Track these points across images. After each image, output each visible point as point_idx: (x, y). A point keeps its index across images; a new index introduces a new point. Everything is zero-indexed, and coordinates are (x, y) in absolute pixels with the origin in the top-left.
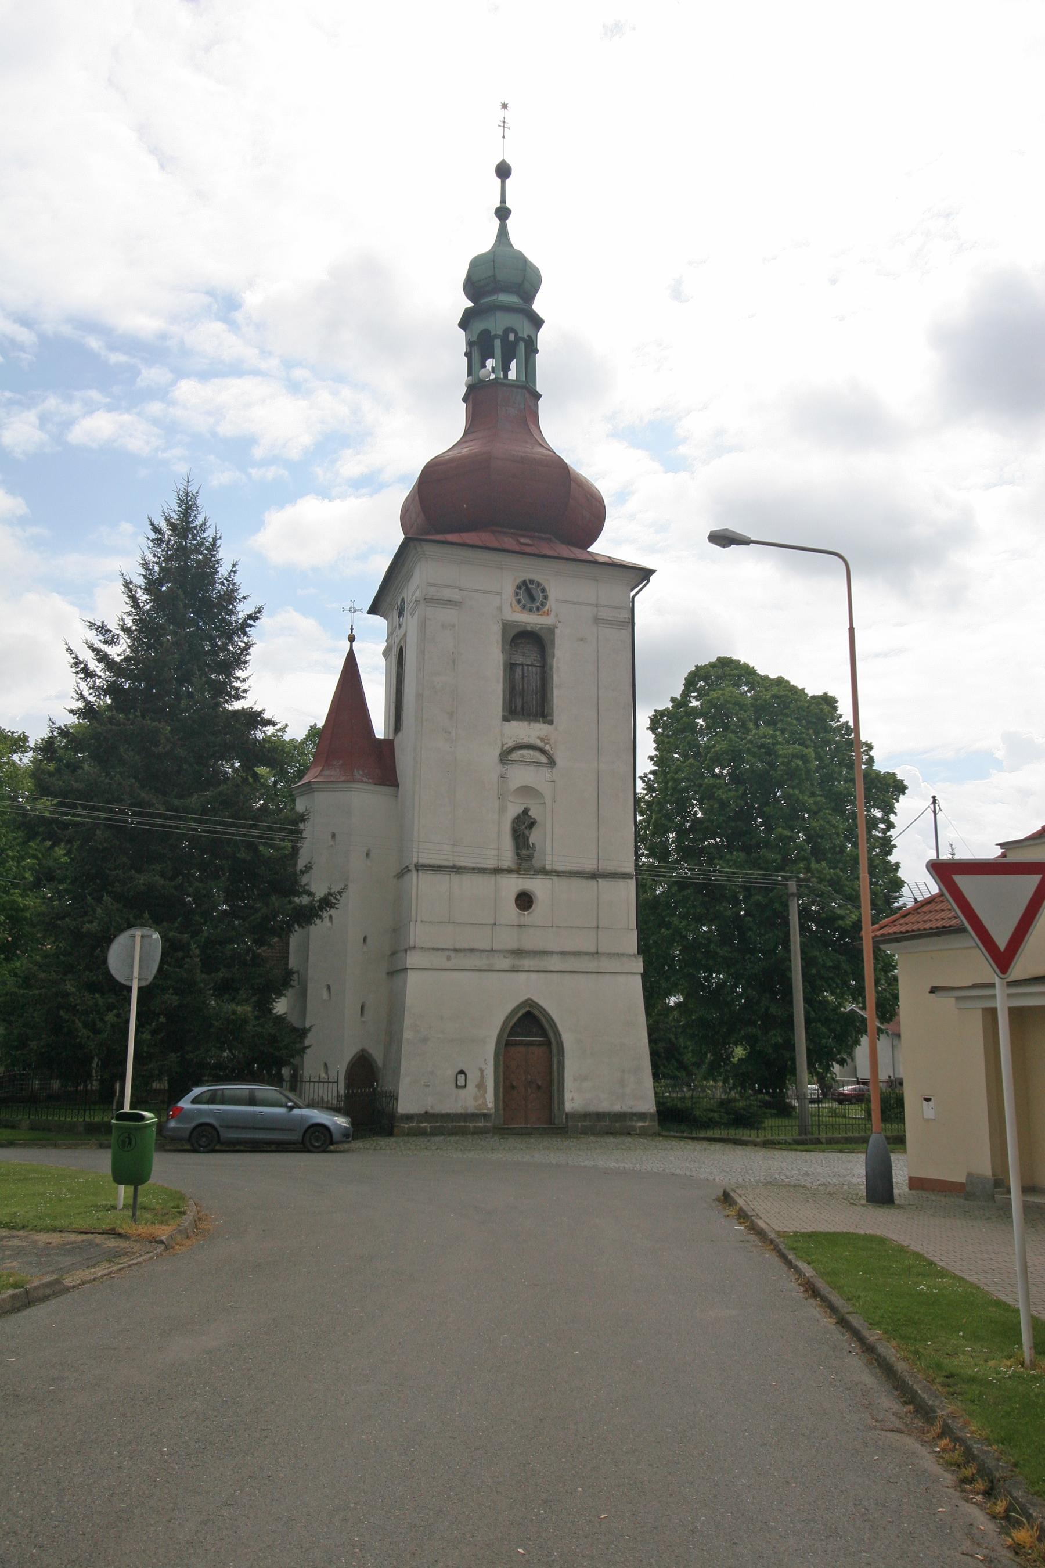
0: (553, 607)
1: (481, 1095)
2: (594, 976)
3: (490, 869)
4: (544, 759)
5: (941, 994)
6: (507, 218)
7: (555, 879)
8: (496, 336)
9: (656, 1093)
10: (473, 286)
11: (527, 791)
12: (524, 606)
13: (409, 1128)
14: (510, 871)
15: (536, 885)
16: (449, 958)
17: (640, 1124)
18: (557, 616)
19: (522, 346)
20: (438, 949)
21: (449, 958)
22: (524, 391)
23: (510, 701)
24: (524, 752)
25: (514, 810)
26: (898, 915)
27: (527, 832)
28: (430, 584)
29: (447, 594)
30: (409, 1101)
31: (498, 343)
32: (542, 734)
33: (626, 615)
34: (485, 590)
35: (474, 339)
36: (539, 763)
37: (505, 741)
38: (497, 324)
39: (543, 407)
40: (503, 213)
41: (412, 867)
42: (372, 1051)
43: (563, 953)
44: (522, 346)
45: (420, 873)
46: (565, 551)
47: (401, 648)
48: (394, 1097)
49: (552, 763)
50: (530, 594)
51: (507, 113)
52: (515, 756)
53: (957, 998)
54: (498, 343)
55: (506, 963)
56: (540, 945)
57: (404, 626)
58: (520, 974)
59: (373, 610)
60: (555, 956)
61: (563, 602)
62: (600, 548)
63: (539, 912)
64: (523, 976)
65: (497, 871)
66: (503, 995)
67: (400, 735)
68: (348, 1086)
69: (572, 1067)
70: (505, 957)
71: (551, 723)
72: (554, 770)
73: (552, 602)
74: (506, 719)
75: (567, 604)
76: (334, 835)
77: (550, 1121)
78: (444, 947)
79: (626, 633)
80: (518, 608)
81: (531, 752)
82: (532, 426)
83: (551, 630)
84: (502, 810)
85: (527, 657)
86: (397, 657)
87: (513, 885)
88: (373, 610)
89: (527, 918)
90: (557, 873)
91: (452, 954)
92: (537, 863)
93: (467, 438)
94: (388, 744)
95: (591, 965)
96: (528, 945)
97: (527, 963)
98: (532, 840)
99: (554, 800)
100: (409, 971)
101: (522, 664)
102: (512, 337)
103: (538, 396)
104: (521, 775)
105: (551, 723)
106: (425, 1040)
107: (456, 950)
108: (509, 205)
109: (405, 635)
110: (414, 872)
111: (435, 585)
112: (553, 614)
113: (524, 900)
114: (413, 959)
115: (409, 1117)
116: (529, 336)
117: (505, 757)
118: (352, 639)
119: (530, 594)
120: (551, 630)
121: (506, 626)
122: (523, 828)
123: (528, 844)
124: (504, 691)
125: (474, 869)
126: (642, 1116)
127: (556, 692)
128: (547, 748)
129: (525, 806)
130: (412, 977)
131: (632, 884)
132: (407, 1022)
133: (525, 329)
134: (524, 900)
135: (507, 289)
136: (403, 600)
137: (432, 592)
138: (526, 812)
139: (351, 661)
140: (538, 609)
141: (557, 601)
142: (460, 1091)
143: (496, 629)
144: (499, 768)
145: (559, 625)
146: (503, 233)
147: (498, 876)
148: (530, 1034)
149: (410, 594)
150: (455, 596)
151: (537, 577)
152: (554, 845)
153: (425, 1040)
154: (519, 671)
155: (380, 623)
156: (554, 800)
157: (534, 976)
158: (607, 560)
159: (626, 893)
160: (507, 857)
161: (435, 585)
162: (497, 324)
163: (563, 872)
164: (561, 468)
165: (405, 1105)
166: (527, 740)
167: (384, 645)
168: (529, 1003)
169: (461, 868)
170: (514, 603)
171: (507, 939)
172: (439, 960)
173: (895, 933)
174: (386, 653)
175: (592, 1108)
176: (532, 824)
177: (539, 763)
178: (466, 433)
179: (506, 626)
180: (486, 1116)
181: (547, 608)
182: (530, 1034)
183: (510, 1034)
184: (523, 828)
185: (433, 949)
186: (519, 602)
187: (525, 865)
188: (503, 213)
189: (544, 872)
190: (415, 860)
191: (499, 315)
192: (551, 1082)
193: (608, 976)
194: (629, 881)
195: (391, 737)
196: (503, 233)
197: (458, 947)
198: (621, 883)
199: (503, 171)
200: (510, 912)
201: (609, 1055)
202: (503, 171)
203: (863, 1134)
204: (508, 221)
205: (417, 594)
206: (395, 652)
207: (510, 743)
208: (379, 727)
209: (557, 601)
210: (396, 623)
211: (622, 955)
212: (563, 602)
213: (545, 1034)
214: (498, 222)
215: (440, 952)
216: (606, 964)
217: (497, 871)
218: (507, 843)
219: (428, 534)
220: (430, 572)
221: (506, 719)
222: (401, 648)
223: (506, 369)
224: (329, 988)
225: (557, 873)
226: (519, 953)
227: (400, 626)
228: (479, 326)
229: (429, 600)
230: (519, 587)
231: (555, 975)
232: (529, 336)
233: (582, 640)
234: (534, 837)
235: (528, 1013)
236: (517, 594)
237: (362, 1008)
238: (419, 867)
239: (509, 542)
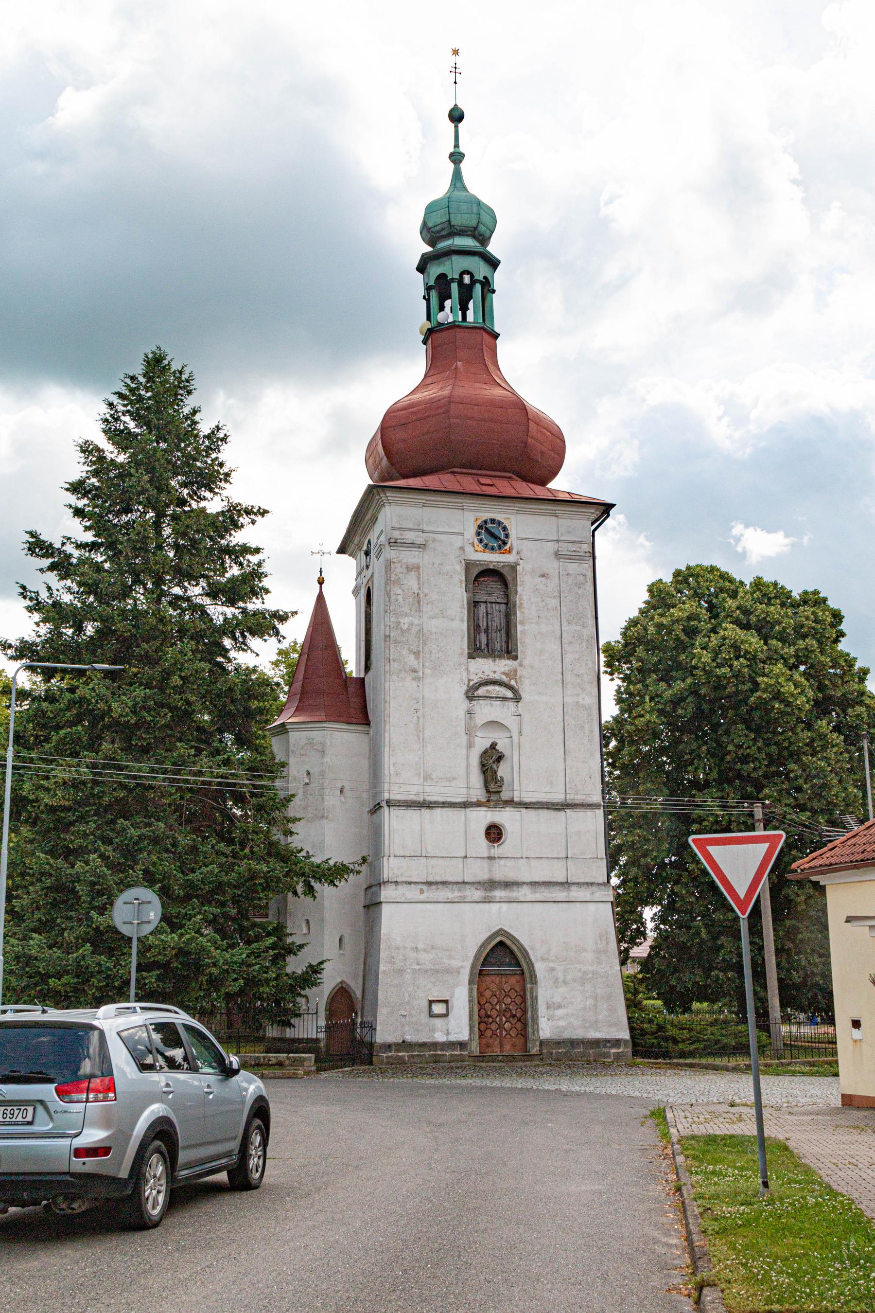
0: (515, 545)
1: (458, 1026)
2: (565, 905)
3: (459, 803)
4: (509, 694)
5: (855, 923)
6: (461, 162)
7: (524, 810)
8: (453, 280)
9: (629, 1018)
10: (431, 233)
11: (493, 724)
12: (486, 546)
13: (387, 1057)
14: (478, 804)
15: (505, 817)
16: (422, 891)
17: (613, 1051)
18: (518, 553)
19: (478, 287)
20: (410, 883)
21: (422, 891)
22: (482, 331)
23: (475, 637)
24: (490, 688)
25: (482, 743)
26: (826, 849)
27: (495, 766)
28: (393, 528)
29: (410, 536)
30: (386, 1031)
31: (454, 287)
32: (506, 669)
33: (586, 547)
34: (445, 531)
35: (432, 283)
36: (504, 699)
37: (472, 677)
38: (453, 267)
39: (502, 347)
40: (456, 157)
41: (384, 804)
42: (349, 982)
43: (534, 884)
44: (478, 287)
45: (392, 809)
46: (526, 489)
47: (369, 588)
48: (373, 1029)
49: (517, 699)
50: (493, 535)
51: (458, 59)
52: (481, 691)
53: (871, 927)
54: (454, 287)
55: (478, 894)
56: (512, 876)
57: (371, 568)
58: (491, 904)
59: (342, 550)
60: (525, 887)
61: (522, 539)
62: (560, 484)
63: (506, 848)
64: (494, 907)
65: (465, 805)
66: (468, 928)
67: (370, 673)
68: (329, 1017)
69: (545, 993)
70: (476, 889)
71: (515, 658)
72: (520, 704)
73: (512, 541)
74: (471, 656)
75: (530, 535)
76: (308, 773)
77: (525, 1049)
78: (417, 880)
79: (587, 566)
80: (480, 547)
81: (497, 688)
82: (491, 368)
83: (513, 568)
84: (470, 745)
85: (492, 591)
86: (367, 598)
87: (483, 817)
88: (342, 550)
89: (496, 851)
90: (527, 806)
91: (425, 887)
92: (505, 795)
93: (429, 380)
94: (361, 681)
95: (561, 895)
96: (498, 876)
97: (499, 894)
98: (499, 774)
99: (520, 734)
100: (383, 905)
101: (486, 602)
102: (467, 279)
103: (496, 336)
104: (486, 711)
105: (515, 658)
106: (401, 972)
107: (429, 884)
108: (462, 149)
109: (372, 576)
110: (386, 809)
111: (400, 529)
112: (514, 552)
113: (494, 833)
114: (386, 893)
115: (389, 1047)
116: (485, 278)
117: (471, 694)
118: (321, 582)
119: (493, 535)
120: (513, 568)
121: (469, 565)
122: (491, 761)
123: (496, 778)
124: (469, 629)
125: (443, 803)
126: (617, 1043)
127: (519, 628)
128: (513, 683)
129: (493, 740)
130: (386, 909)
131: (600, 813)
132: (383, 954)
133: (481, 269)
134: (494, 833)
135: (462, 232)
136: (369, 542)
137: (396, 534)
138: (493, 746)
139: (320, 599)
140: (500, 548)
141: (518, 538)
142: (438, 1022)
143: (460, 569)
144: (465, 704)
145: (521, 562)
146: (457, 176)
147: (468, 810)
148: (502, 964)
149: (376, 535)
150: (419, 538)
151: (498, 517)
152: (525, 777)
153: (401, 972)
154: (482, 609)
155: (349, 565)
156: (520, 734)
157: (505, 906)
158: (567, 497)
159: (591, 826)
160: (478, 792)
161: (400, 529)
162: (453, 267)
163: (531, 803)
164: (521, 406)
165: (384, 1034)
166: (492, 676)
167: (353, 584)
168: (501, 932)
169: (431, 803)
170: (476, 542)
171: (479, 871)
172: (412, 893)
173: (821, 865)
174: (356, 592)
175: (566, 1035)
176: (500, 758)
177: (504, 699)
178: (426, 375)
179: (469, 565)
180: (462, 1045)
181: (507, 547)
182: (502, 964)
183: (483, 965)
184: (491, 761)
185: (406, 882)
186: (481, 541)
187: (494, 797)
188: (456, 157)
189: (510, 803)
190: (386, 796)
191: (455, 258)
192: (525, 1012)
193: (578, 904)
194: (597, 811)
195: (362, 676)
196: (457, 176)
197: (430, 879)
198: (589, 813)
199: (456, 116)
200: (482, 845)
201: (582, 980)
202: (456, 116)
203: (538, 1044)
204: (462, 165)
205: (382, 538)
206: (363, 592)
207: (476, 680)
208: (352, 665)
209: (518, 538)
210: (364, 564)
211: (592, 884)
212: (522, 539)
213: (518, 964)
214: (452, 166)
215: (413, 886)
216: (576, 893)
217: (465, 805)
218: (476, 779)
219: (392, 479)
220: (394, 514)
221: (471, 656)
222: (369, 588)
223: (464, 309)
224: (308, 922)
225: (527, 806)
226: (491, 884)
227: (367, 567)
228: (435, 270)
229: (393, 543)
230: (480, 527)
231: (526, 904)
232: (485, 278)
233: (543, 576)
234: (502, 771)
235: (501, 944)
236: (478, 534)
237: (340, 940)
238: (389, 803)
239: (469, 483)
